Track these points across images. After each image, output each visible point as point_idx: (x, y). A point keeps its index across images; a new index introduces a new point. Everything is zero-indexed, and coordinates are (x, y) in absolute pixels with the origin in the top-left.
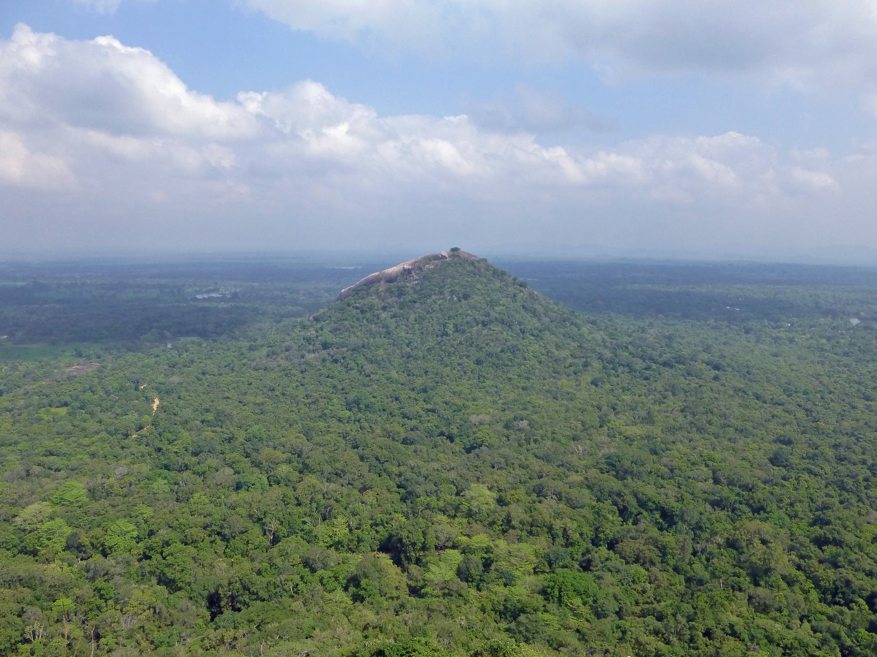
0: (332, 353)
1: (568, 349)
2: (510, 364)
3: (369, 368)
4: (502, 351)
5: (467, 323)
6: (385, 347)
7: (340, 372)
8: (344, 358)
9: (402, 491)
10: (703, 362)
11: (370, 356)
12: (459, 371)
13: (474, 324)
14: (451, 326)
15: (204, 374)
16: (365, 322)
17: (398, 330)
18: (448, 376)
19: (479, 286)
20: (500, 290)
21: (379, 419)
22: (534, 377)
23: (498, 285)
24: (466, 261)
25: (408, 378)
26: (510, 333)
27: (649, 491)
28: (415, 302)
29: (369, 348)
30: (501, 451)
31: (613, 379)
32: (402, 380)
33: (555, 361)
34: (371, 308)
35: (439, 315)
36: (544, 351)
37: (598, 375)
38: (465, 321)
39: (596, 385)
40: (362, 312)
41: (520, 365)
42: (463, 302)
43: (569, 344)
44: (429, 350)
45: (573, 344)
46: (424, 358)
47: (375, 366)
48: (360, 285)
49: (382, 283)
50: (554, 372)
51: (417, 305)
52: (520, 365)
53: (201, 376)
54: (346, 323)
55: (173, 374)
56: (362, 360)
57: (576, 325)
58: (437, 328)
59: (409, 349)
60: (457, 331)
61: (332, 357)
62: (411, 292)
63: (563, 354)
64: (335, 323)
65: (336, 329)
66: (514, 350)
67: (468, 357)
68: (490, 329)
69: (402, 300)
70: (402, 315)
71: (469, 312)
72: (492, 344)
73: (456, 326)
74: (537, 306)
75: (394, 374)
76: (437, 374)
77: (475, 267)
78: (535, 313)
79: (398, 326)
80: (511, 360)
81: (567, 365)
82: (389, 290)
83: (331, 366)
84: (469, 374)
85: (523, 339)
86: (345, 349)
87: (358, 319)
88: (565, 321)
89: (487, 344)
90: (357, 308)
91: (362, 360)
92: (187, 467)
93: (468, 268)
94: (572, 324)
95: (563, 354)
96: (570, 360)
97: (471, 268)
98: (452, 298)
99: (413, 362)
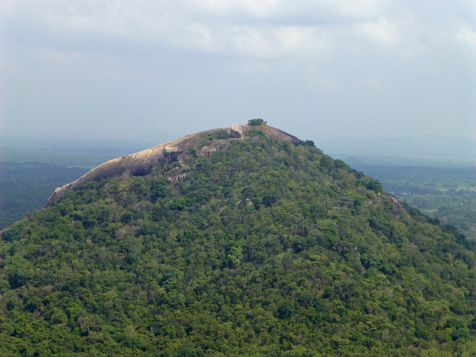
0: (25, 294)
1: (448, 298)
2: (338, 317)
3: (87, 319)
4: (326, 296)
5: (268, 245)
6: (121, 285)
7: (35, 327)
8: (46, 303)
11: (91, 299)
12: (246, 328)
13: (279, 247)
14: (239, 250)
16: (89, 241)
17: (146, 257)
18: (226, 337)
19: (292, 183)
20: (331, 192)
22: (379, 342)
23: (328, 183)
24: (273, 141)
25: (155, 339)
26: (342, 266)
28: (180, 209)
29: (91, 286)
32: (144, 343)
33: (422, 317)
34: (102, 218)
35: (220, 231)
36: (402, 300)
38: (263, 241)
40: (87, 225)
41: (357, 320)
42: (264, 209)
43: (449, 290)
44: (197, 291)
45: (456, 290)
46: (187, 304)
47: (99, 318)
48: (86, 180)
49: (126, 175)
50: (416, 335)
51: (184, 214)
52: (357, 320)
54: (54, 242)
56: (76, 307)
58: (214, 252)
59: (161, 290)
60: (248, 259)
61: (25, 300)
62: (174, 192)
63: (436, 306)
64: (36, 242)
65: (37, 254)
66: (346, 295)
67: (265, 304)
68: (307, 257)
69: (157, 204)
70: (156, 231)
71: (272, 226)
72: (309, 283)
73: (246, 250)
74: (396, 223)
75: (131, 331)
76: (208, 333)
77: (289, 152)
78: (391, 236)
79: (147, 249)
80: (341, 312)
81: (442, 324)
82: (136, 189)
83: (22, 316)
84: (266, 334)
85: (366, 276)
86: (49, 288)
87: (76, 237)
88: (445, 251)
89: (299, 284)
90: (77, 218)
91: (76, 307)
93: (277, 154)
94: (458, 256)
95: (436, 306)
96: (449, 316)
97: (282, 154)
98: (244, 202)
99: (167, 312)
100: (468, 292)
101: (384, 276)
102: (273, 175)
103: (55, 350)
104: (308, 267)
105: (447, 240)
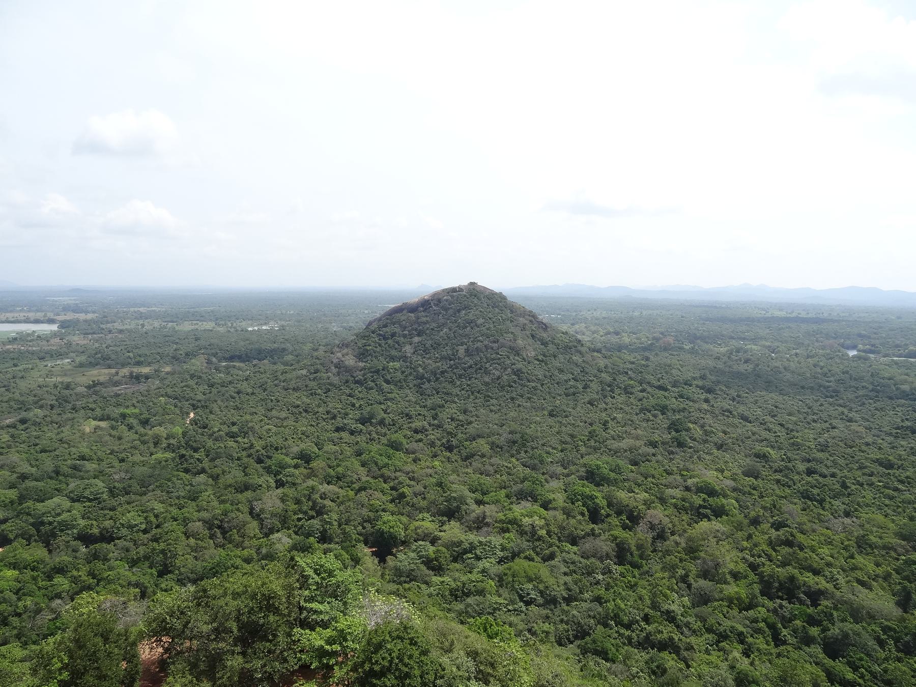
9: (394, 492)
11: (388, 377)
15: (238, 393)
27: (622, 495)
31: (609, 400)
39: (592, 405)
55: (98, 581)
57: (580, 353)
90: (380, 335)
91: (380, 381)
92: (203, 471)
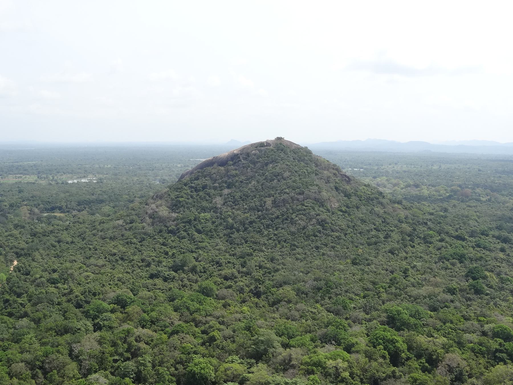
9: (205, 336)
10: (494, 236)
11: (200, 227)
12: (274, 240)
15: (59, 242)
21: (199, 279)
27: (422, 340)
30: (298, 306)
37: (396, 246)
49: (215, 165)
53: (56, 244)
71: (287, 190)
90: (192, 187)
91: (192, 231)
96: (373, 233)
100: (383, 220)
101: (341, 213)
102: (287, 165)
103: (182, 252)
104: (305, 210)
105: (511, 161)
